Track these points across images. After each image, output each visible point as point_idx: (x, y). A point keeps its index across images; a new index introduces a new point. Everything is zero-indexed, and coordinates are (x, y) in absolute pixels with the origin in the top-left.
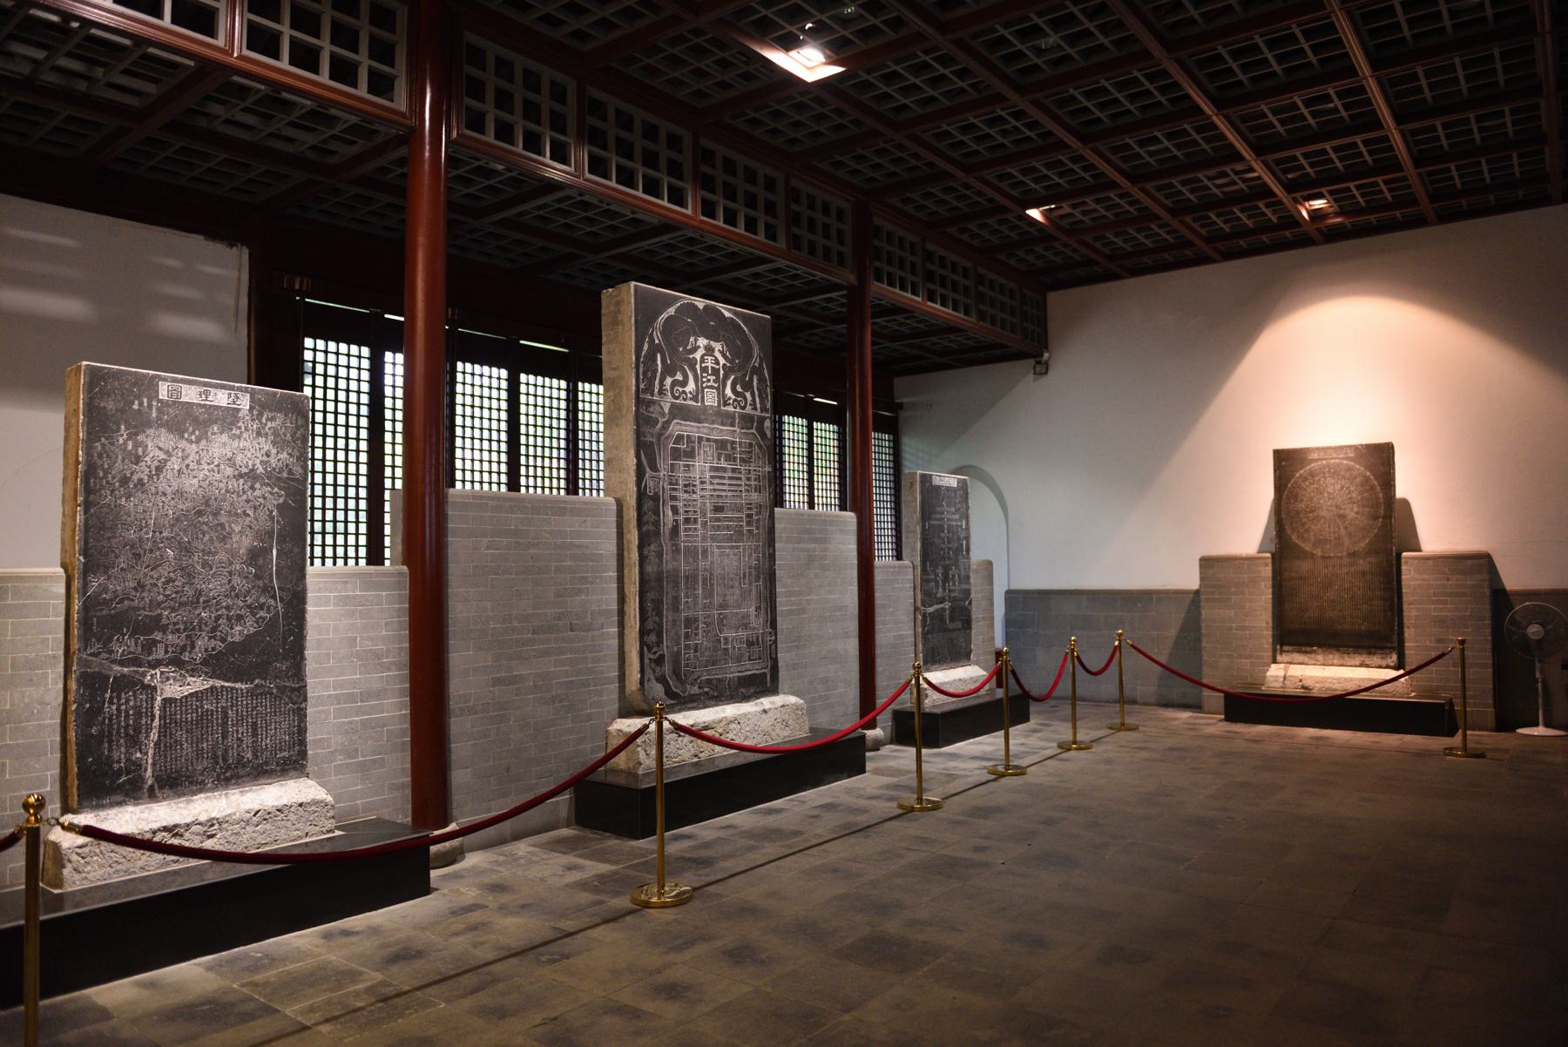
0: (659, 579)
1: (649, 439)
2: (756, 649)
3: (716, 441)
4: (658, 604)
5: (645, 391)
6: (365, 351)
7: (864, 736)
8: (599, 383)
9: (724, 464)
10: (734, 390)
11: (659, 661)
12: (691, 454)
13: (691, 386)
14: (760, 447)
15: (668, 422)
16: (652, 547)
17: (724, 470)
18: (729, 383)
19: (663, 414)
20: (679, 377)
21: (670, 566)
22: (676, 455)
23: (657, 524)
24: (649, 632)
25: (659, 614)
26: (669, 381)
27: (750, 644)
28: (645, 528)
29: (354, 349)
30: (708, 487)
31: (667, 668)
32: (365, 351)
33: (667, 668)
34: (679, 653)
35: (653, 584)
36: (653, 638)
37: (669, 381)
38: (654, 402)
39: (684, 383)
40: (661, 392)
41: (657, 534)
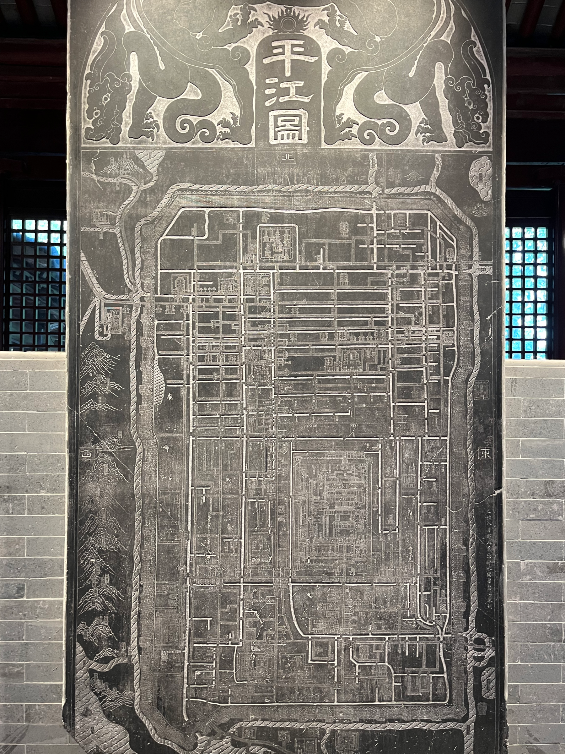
0: (123, 510)
1: (103, 229)
2: (425, 674)
3: (300, 220)
4: (118, 566)
5: (92, 135)
6: (542, 232)
7: (66, 219)
8: (62, 217)
9: (323, 265)
10: (363, 101)
11: (119, 677)
12: (226, 250)
13: (229, 107)
14: (453, 223)
15: (158, 191)
16: (105, 445)
17: (328, 279)
18: (349, 91)
19: (145, 176)
20: (192, 93)
21: (154, 482)
22: (178, 254)
23: (120, 398)
24: (90, 617)
25: (120, 579)
26: (160, 106)
27: (405, 661)
28: (85, 409)
29: (529, 232)
30: (273, 316)
31: (138, 694)
32: (542, 232)
33: (138, 694)
34: (173, 665)
35: (104, 518)
36: (102, 628)
37: (160, 106)
38: (118, 155)
39: (210, 102)
40: (141, 130)
41: (120, 418)
